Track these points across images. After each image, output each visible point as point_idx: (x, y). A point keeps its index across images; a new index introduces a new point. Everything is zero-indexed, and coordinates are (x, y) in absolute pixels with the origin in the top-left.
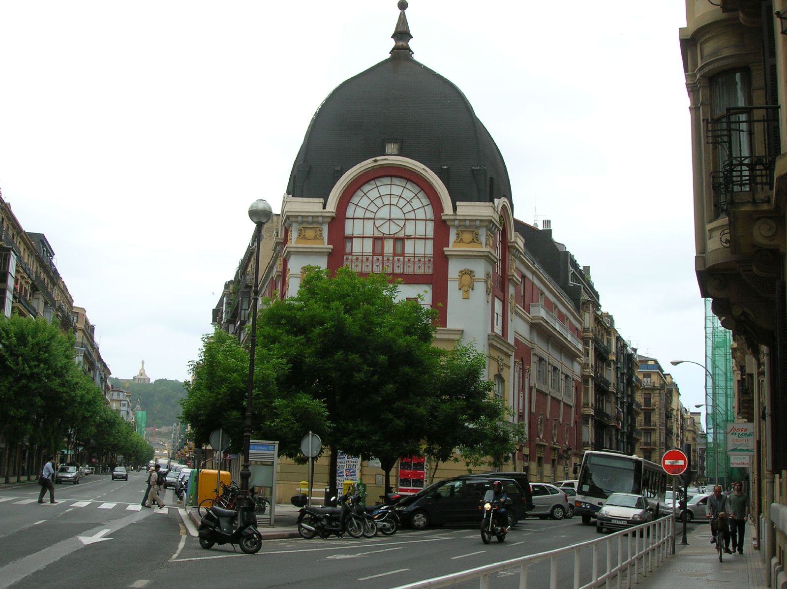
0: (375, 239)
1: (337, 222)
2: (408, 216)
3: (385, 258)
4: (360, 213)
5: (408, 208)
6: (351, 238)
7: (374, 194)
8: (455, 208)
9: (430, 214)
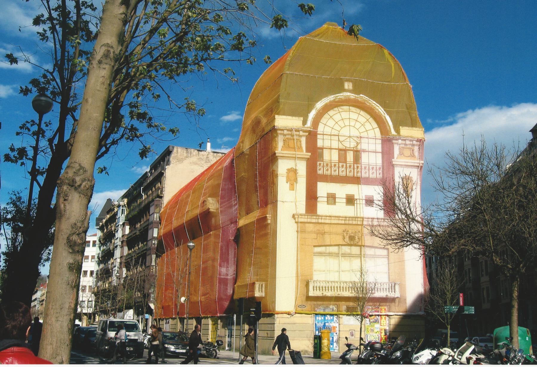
0: (340, 150)
1: (312, 136)
2: (362, 135)
3: (348, 165)
4: (328, 130)
5: (362, 129)
6: (322, 149)
7: (337, 117)
8: (398, 131)
9: (378, 134)
